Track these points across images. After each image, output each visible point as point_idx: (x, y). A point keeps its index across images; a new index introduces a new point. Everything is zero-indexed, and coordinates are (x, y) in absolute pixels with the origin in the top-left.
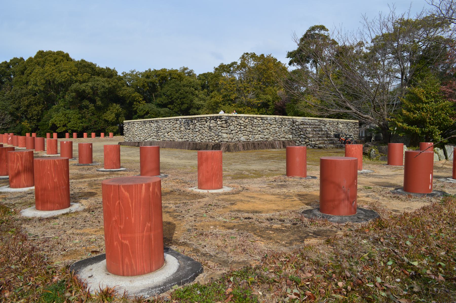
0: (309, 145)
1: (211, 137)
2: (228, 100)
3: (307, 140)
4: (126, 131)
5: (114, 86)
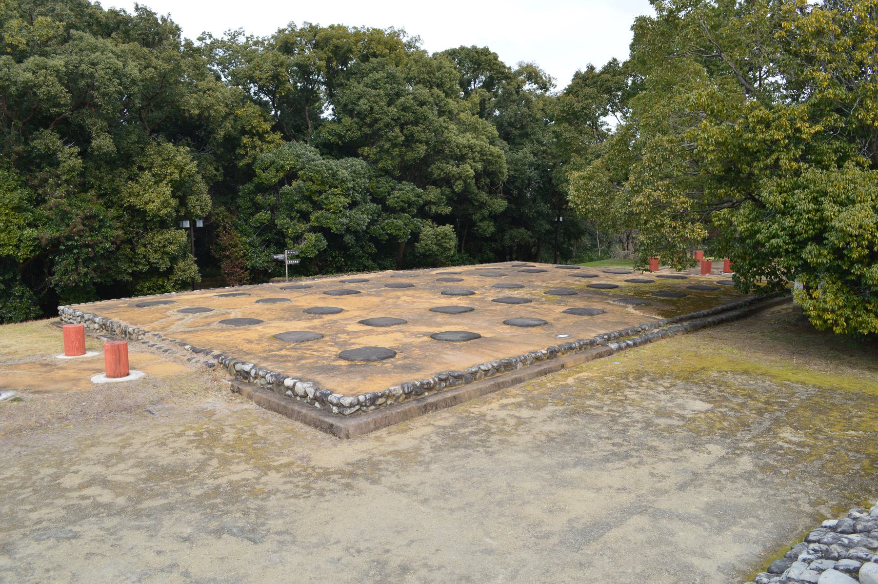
5: (163, 76)
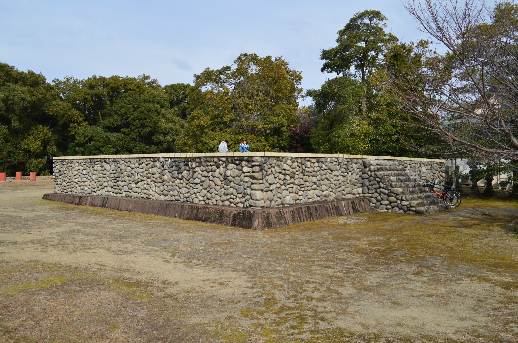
0: (397, 206)
1: (228, 197)
2: (220, 123)
3: (392, 198)
4: (57, 175)
5: (39, 100)
